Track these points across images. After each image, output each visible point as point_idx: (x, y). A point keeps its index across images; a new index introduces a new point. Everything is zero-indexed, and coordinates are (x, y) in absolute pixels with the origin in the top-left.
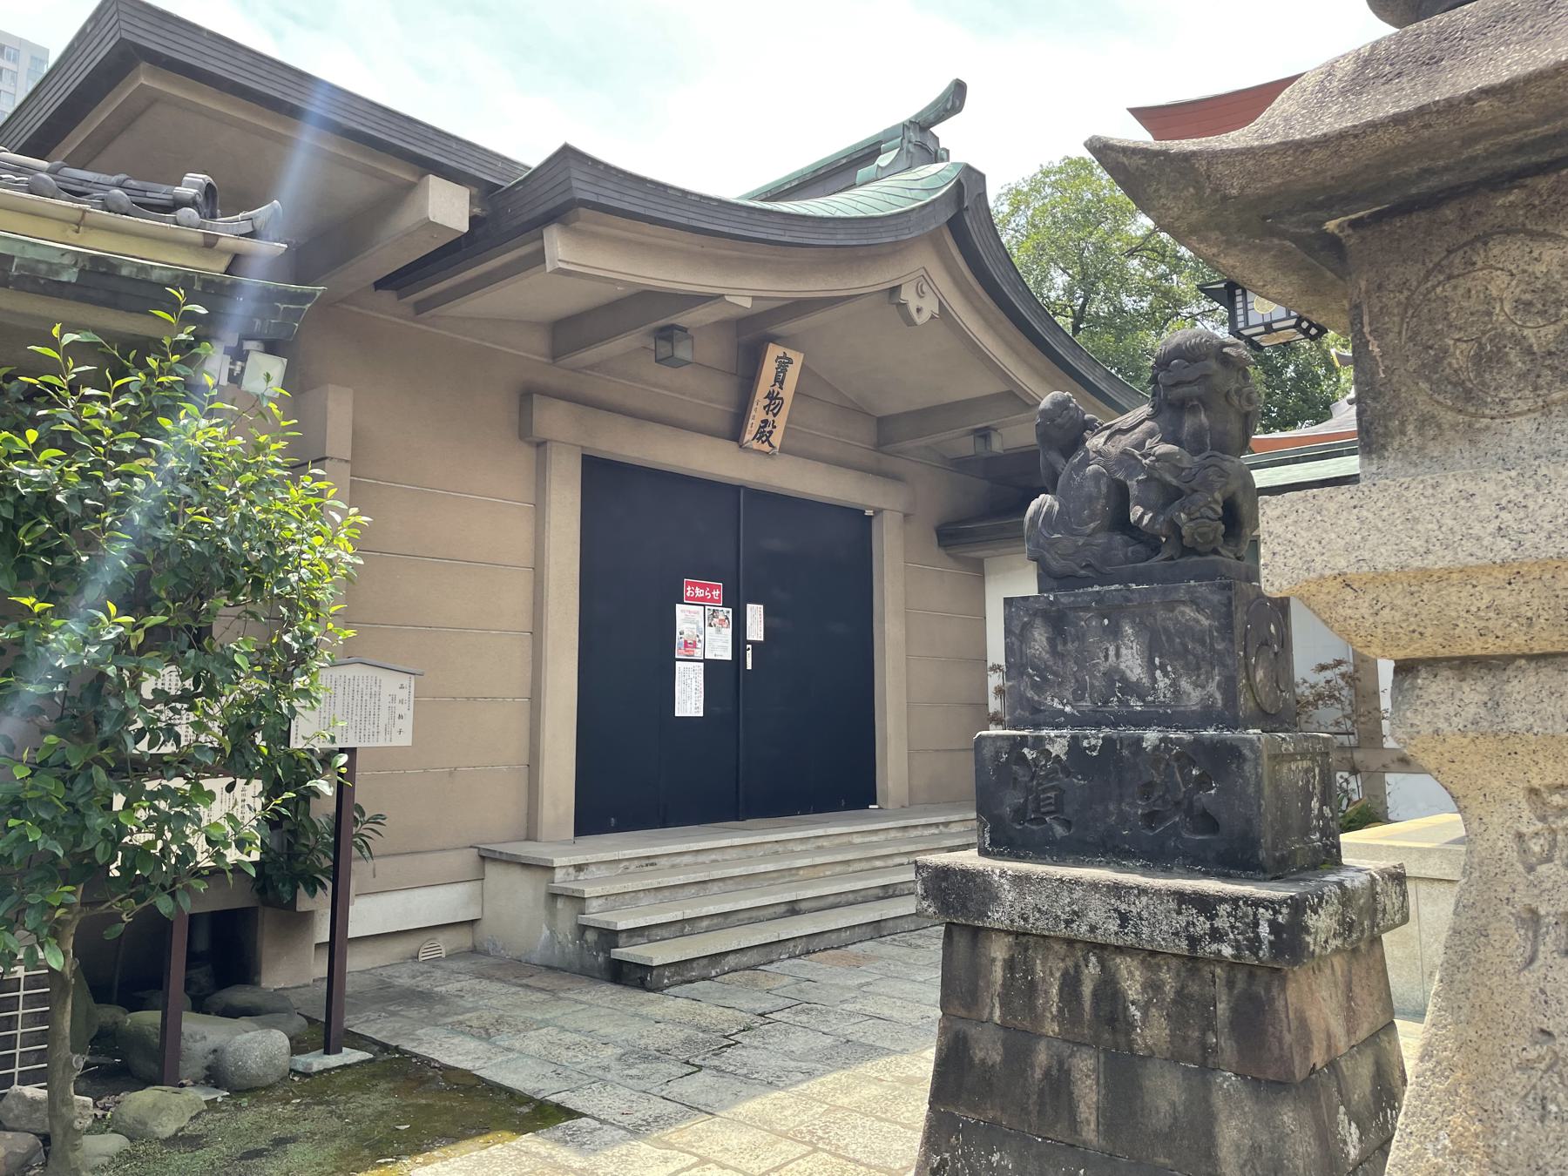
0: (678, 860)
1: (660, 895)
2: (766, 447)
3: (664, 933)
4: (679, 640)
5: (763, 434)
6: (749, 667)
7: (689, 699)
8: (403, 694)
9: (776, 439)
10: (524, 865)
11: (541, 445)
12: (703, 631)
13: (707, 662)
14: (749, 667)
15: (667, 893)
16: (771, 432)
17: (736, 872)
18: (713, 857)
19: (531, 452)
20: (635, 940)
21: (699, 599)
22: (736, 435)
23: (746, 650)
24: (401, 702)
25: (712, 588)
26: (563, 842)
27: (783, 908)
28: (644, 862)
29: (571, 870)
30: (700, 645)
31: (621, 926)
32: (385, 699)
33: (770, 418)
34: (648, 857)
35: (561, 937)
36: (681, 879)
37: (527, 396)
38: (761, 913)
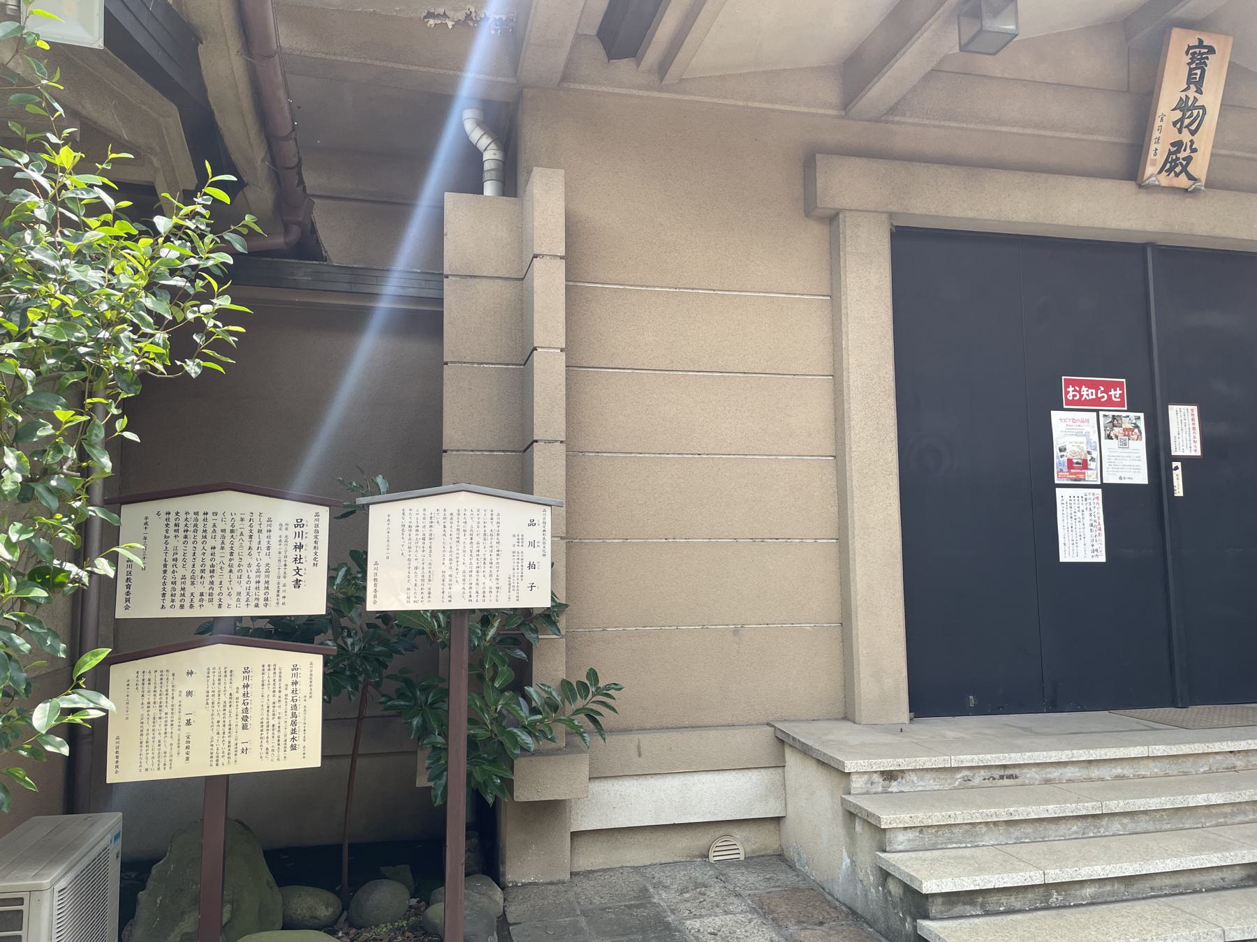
0: (1055, 773)
1: (1016, 832)
2: (1183, 181)
3: (1015, 902)
4: (1059, 460)
5: (1176, 162)
6: (1179, 491)
7: (1081, 535)
8: (535, 534)
9: (1200, 167)
10: (819, 761)
11: (832, 219)
12: (1097, 447)
13: (1103, 486)
14: (1179, 491)
15: (1029, 829)
16: (1189, 159)
17: (1153, 803)
18: (1118, 771)
19: (818, 230)
20: (959, 909)
21: (1087, 402)
22: (1132, 171)
23: (1170, 471)
24: (532, 544)
25: (1108, 387)
26: (888, 729)
27: (1239, 874)
28: (997, 773)
29: (876, 778)
30: (1092, 465)
31: (929, 887)
32: (507, 544)
33: (1186, 137)
34: (1005, 767)
35: (861, 875)
36: (1052, 810)
37: (808, 163)
38: (1196, 880)
